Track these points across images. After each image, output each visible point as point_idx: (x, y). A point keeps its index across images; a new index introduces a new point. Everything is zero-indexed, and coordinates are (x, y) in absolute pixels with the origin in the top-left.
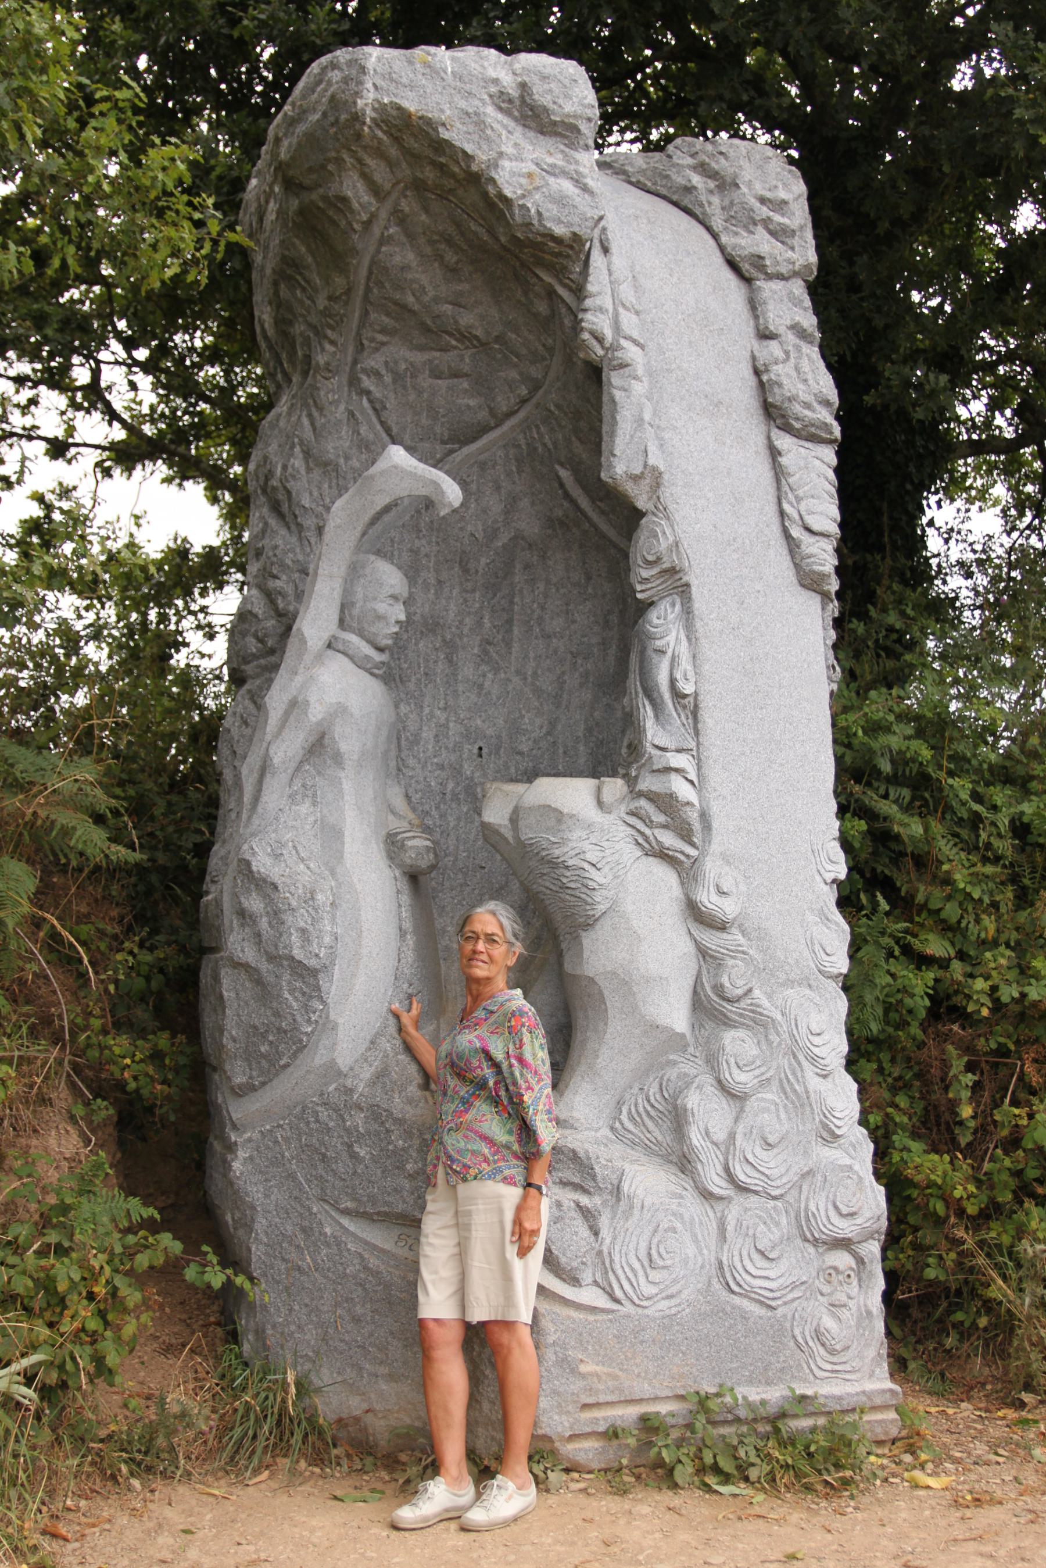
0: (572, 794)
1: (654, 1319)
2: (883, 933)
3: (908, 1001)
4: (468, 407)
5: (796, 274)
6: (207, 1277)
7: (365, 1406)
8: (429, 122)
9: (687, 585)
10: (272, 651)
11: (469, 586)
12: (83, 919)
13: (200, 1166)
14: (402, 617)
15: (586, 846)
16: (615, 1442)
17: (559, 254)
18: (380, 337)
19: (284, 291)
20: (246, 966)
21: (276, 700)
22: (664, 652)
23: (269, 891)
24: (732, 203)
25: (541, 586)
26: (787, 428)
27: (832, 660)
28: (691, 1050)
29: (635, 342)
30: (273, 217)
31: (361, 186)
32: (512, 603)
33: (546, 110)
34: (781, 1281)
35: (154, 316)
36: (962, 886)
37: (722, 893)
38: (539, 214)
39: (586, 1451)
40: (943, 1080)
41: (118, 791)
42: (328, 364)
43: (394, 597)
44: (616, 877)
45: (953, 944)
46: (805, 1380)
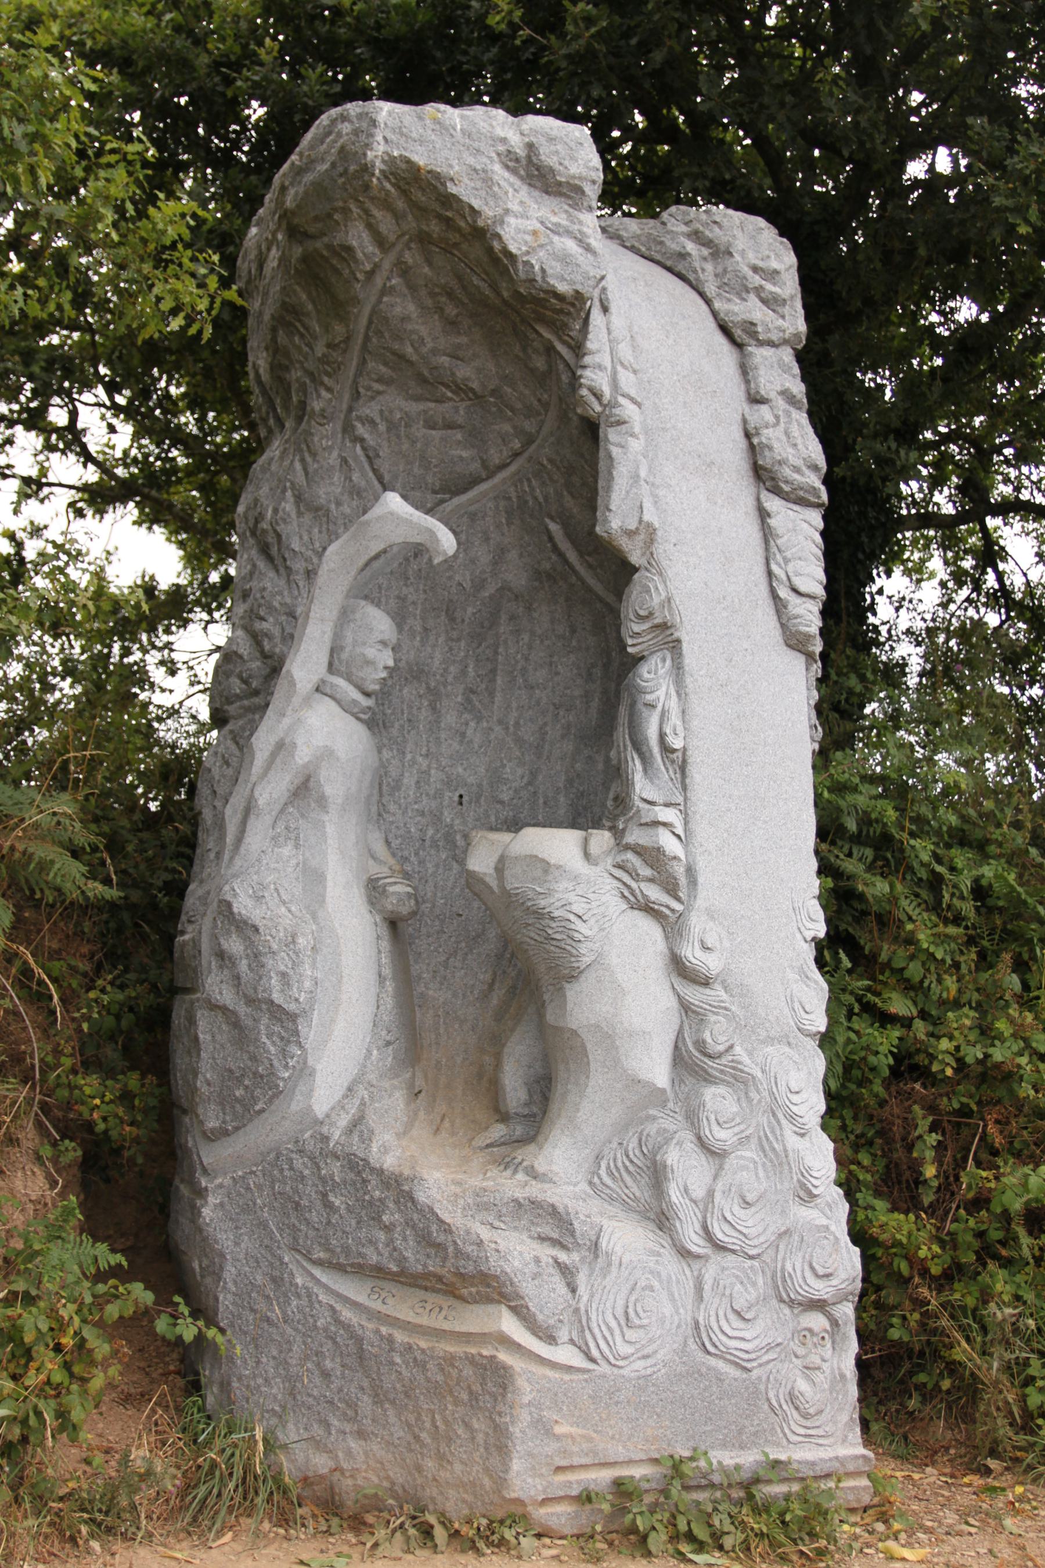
0: (559, 845)
1: (629, 1380)
2: (844, 990)
3: (872, 1059)
4: (461, 458)
5: (785, 342)
6: (178, 1330)
7: (331, 1464)
8: (437, 176)
9: (678, 641)
10: (256, 693)
11: (455, 634)
12: (55, 955)
13: (164, 1209)
14: (391, 663)
15: (572, 897)
16: (588, 1507)
17: (561, 311)
18: (377, 386)
19: (282, 338)
20: (224, 1009)
21: (263, 741)
22: (654, 707)
23: (250, 933)
24: (725, 271)
25: (526, 637)
26: (776, 491)
27: (815, 720)
28: (671, 1105)
29: (633, 400)
30: (275, 264)
31: (366, 236)
32: (496, 653)
33: (552, 170)
34: (756, 1342)
35: (133, 365)
36: (925, 946)
37: (706, 948)
38: (543, 270)
39: (559, 1516)
40: (904, 1139)
41: (93, 827)
42: (323, 410)
43: (383, 643)
44: (602, 930)
45: (915, 1003)
46: (778, 1445)
